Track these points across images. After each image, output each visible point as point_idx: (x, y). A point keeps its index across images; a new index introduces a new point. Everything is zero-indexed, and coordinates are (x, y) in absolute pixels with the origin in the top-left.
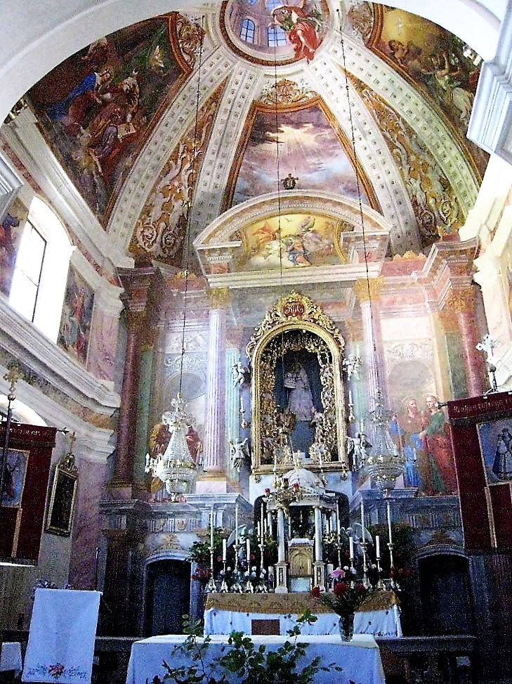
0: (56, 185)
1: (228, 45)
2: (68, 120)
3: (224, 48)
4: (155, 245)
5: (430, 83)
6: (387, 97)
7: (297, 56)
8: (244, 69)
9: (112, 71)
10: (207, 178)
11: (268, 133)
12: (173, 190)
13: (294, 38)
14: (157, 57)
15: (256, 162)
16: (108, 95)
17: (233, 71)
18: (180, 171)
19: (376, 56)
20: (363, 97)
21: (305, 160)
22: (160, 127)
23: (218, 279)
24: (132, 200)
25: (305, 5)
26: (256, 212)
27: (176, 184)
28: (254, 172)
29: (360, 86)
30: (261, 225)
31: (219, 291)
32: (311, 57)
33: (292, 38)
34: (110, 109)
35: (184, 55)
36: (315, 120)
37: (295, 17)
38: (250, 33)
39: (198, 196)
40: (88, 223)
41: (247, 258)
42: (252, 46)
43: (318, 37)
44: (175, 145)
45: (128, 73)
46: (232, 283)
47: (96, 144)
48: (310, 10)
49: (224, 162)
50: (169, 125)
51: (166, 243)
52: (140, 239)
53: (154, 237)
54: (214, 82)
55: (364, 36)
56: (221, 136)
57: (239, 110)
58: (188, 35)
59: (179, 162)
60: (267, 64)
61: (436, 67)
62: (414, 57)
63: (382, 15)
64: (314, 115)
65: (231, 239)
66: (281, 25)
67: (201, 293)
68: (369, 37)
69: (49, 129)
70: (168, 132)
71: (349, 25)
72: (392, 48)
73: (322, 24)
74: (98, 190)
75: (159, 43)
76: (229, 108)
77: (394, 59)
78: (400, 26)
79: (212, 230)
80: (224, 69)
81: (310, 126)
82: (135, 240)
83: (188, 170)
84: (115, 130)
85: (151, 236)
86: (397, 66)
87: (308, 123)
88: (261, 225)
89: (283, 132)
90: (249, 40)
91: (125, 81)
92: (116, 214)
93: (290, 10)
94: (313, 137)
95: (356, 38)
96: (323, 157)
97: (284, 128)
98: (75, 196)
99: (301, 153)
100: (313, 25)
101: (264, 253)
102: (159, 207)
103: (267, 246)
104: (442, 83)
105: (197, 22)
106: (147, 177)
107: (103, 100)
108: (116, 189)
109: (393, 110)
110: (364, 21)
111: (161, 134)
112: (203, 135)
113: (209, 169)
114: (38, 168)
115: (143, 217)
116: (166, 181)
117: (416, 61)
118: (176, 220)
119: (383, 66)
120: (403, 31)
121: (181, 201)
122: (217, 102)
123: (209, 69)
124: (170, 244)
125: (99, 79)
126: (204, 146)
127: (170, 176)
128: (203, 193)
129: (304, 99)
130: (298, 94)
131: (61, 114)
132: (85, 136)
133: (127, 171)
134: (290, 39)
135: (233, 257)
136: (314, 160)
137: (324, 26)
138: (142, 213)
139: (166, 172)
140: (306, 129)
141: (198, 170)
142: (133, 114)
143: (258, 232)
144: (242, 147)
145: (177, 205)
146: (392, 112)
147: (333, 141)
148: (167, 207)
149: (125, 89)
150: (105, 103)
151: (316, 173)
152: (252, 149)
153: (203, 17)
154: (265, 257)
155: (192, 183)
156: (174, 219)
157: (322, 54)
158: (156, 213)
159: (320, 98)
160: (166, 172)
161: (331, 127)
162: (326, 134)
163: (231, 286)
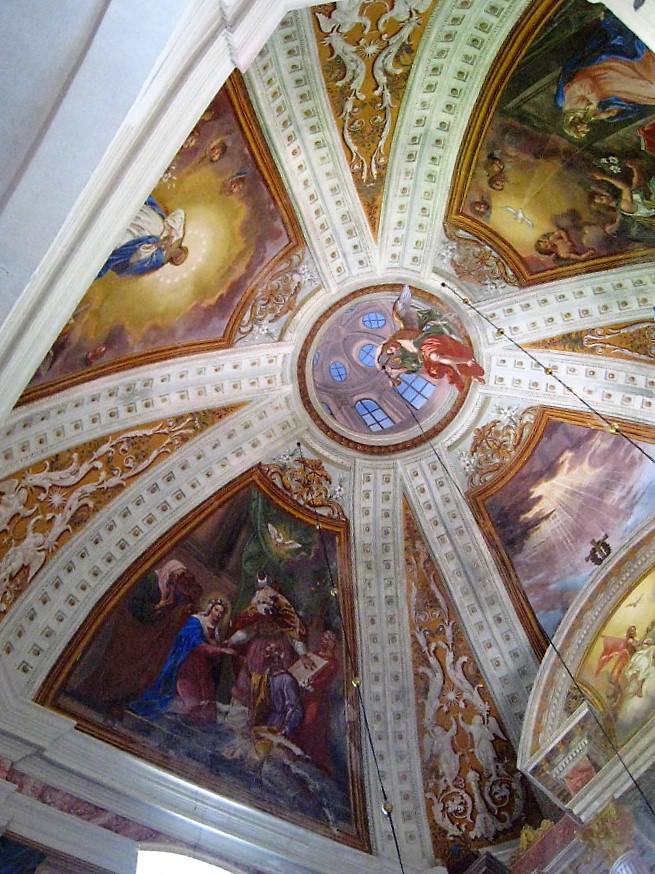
0: (187, 813)
1: (364, 452)
2: (183, 704)
3: (362, 462)
4: (479, 818)
5: (634, 231)
6: (616, 316)
7: (461, 387)
8: (415, 465)
9: (221, 598)
10: (493, 653)
11: (522, 517)
12: (453, 708)
13: (441, 370)
14: (280, 540)
15: (541, 571)
16: (240, 635)
17: (401, 480)
18: (444, 673)
19: (546, 285)
20: (593, 350)
21: (606, 505)
22: (364, 631)
23: (589, 798)
24: (392, 768)
25: (403, 320)
26: (580, 635)
27: (451, 696)
28: (552, 587)
29: (573, 341)
30: (599, 647)
31: (601, 818)
32: (478, 371)
33: (434, 372)
34: (253, 658)
35: (319, 511)
36: (567, 442)
37: (408, 345)
38: (379, 415)
39: (497, 690)
40: (304, 849)
41: (612, 717)
42: (397, 428)
43: (459, 339)
44: (408, 640)
45: (253, 586)
46: (615, 786)
47: (264, 714)
48: (415, 317)
49: (497, 610)
50: (377, 620)
51: (494, 802)
52: (446, 824)
53: (469, 805)
54: (390, 513)
55: (504, 277)
56: (465, 579)
57: (457, 523)
58: (299, 481)
59: (432, 660)
60: (436, 431)
61: (613, 204)
62: (579, 228)
63: (491, 230)
64: (559, 436)
65: (569, 710)
66: (405, 370)
67: (575, 848)
68: (510, 273)
69: (147, 731)
70: (384, 629)
71: (476, 287)
72: (548, 253)
73: (446, 319)
74: (314, 785)
75: (267, 520)
76: (443, 531)
77: (568, 261)
78: (520, 215)
79: (533, 722)
80: (389, 487)
81: (568, 455)
82: (438, 833)
83: (454, 663)
84: (287, 678)
85: (462, 807)
86: (580, 265)
87: (562, 453)
88: (599, 647)
89: (540, 498)
90: (387, 424)
91: (255, 600)
92: (377, 812)
93: (393, 342)
94: (585, 466)
95: (501, 291)
96: (627, 480)
97: (538, 491)
98: (235, 813)
99: (590, 501)
100: (438, 334)
101: (631, 689)
102: (447, 753)
103: (630, 673)
104: (642, 212)
105: (297, 456)
106: (398, 717)
107: (234, 647)
108: (352, 763)
109: (643, 322)
110: (483, 261)
111: (374, 639)
112: (439, 596)
113: (484, 636)
114: (138, 802)
115: (431, 785)
116: (432, 704)
117: (587, 230)
118: (491, 754)
119: (567, 286)
120: (530, 217)
121: (477, 719)
122: (420, 538)
123: (369, 503)
124: (504, 797)
125: (204, 620)
126: (452, 610)
127: (434, 692)
128: (504, 680)
129: (526, 431)
130: (512, 431)
131: (165, 702)
132: (234, 713)
133: (355, 729)
134: (433, 376)
135: (589, 738)
136: (617, 494)
137: (451, 318)
138: (426, 779)
139: (423, 690)
140: (567, 465)
141: (469, 651)
142: (304, 638)
143: (602, 664)
144: (506, 568)
145: (475, 728)
146: (645, 325)
147: (616, 444)
148: (462, 743)
149: (262, 612)
150: (242, 648)
151: (637, 509)
152: (520, 558)
153: (299, 444)
154: (638, 693)
155: (475, 677)
156: (484, 753)
157: (489, 351)
158: (449, 765)
159: (544, 409)
160: (423, 690)
161: (595, 431)
162: (599, 444)
163: (616, 791)
